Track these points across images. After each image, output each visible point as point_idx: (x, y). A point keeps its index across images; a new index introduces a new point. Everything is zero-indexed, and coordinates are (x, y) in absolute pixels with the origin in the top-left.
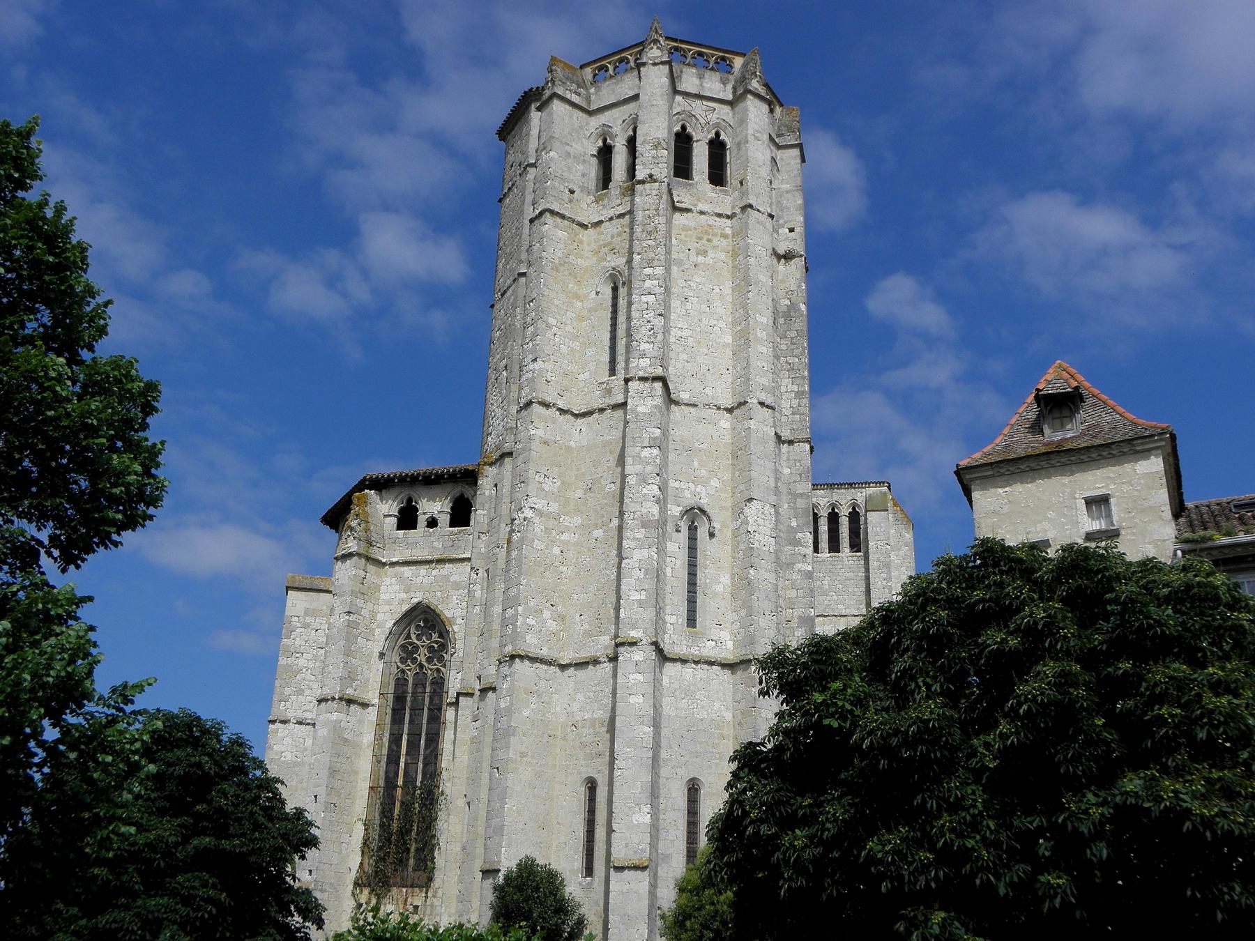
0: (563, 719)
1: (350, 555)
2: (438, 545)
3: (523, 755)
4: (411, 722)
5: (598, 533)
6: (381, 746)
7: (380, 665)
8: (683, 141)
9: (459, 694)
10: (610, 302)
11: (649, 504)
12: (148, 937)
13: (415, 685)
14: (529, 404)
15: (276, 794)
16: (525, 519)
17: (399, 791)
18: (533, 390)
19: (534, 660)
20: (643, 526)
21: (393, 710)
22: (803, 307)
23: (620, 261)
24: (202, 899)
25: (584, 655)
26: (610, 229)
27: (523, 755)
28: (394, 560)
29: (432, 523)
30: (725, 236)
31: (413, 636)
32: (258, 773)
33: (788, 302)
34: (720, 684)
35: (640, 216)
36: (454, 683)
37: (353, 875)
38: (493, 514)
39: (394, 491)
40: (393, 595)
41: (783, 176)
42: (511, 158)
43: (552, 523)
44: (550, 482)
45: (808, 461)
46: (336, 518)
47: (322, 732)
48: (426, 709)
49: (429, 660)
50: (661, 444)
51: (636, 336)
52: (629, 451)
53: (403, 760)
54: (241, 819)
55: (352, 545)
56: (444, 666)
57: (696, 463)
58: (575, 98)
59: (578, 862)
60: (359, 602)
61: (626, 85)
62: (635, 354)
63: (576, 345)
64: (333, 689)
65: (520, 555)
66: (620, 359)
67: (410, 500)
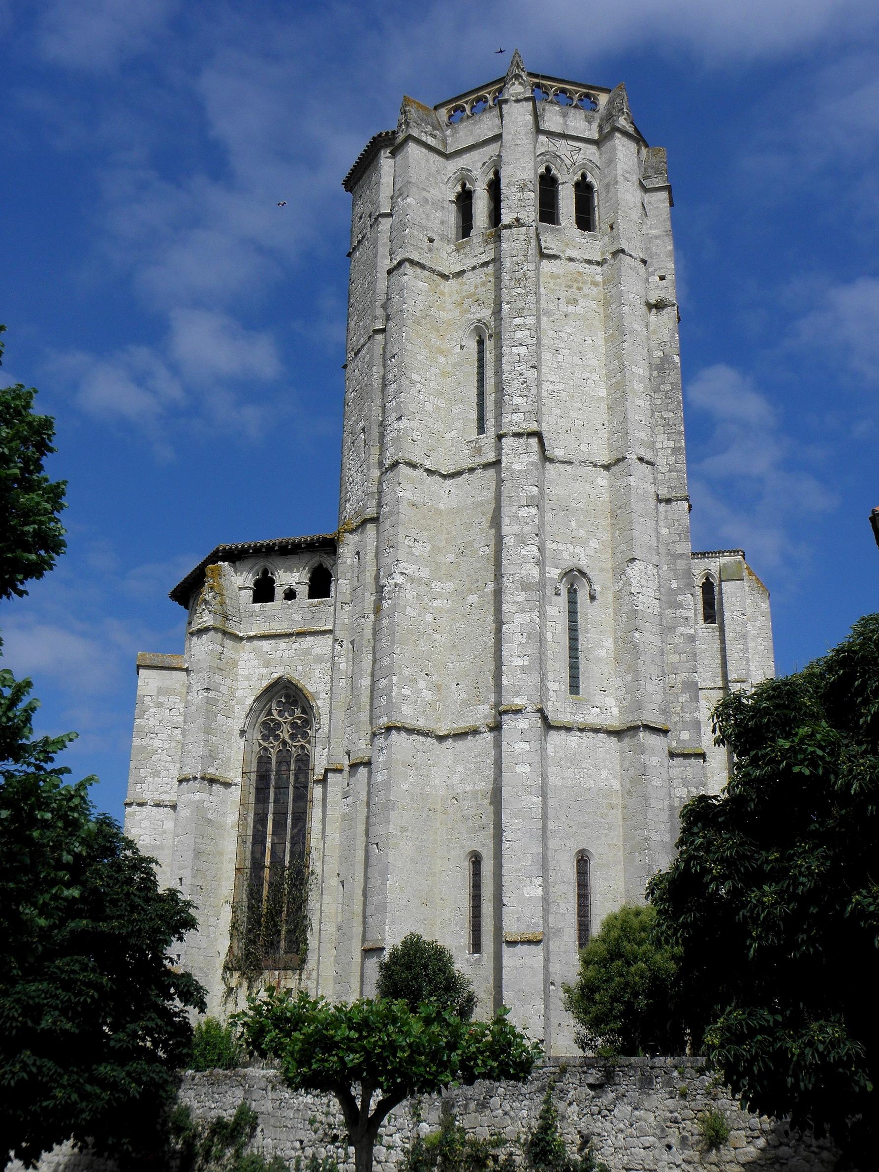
0: (443, 792)
1: (206, 630)
2: (297, 617)
3: (404, 829)
4: (276, 801)
5: (473, 598)
6: (246, 827)
7: (241, 743)
8: (548, 185)
9: (327, 771)
10: (475, 357)
11: (528, 566)
12: (30, 1023)
13: (279, 763)
14: (395, 464)
15: (150, 873)
16: (396, 585)
17: (267, 871)
18: (398, 450)
19: (410, 731)
20: (523, 589)
21: (257, 789)
22: (677, 359)
23: (486, 313)
24: (84, 983)
25: (463, 725)
26: (473, 280)
27: (404, 829)
28: (252, 634)
29: (290, 595)
30: (595, 284)
31: (275, 713)
32: (129, 853)
33: (661, 354)
34: (607, 752)
35: (507, 263)
36: (320, 760)
37: (222, 959)
38: (356, 583)
39: (249, 563)
40: (251, 671)
41: (652, 221)
42: (359, 209)
43: (423, 589)
44: (422, 546)
45: (686, 520)
46: (188, 593)
47: (184, 812)
48: (291, 787)
49: (293, 737)
50: (537, 503)
51: (508, 390)
52: (505, 511)
53: (269, 840)
54: (118, 900)
55: (206, 619)
56: (309, 742)
57: (573, 524)
58: (430, 141)
59: (464, 938)
60: (218, 678)
61: (486, 126)
62: (507, 409)
63: (441, 403)
64: (193, 768)
65: (392, 623)
66: (490, 416)
67: (265, 572)
